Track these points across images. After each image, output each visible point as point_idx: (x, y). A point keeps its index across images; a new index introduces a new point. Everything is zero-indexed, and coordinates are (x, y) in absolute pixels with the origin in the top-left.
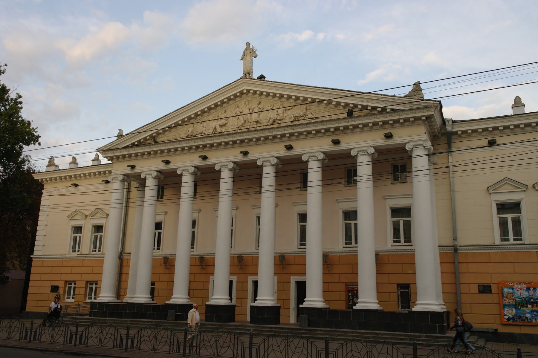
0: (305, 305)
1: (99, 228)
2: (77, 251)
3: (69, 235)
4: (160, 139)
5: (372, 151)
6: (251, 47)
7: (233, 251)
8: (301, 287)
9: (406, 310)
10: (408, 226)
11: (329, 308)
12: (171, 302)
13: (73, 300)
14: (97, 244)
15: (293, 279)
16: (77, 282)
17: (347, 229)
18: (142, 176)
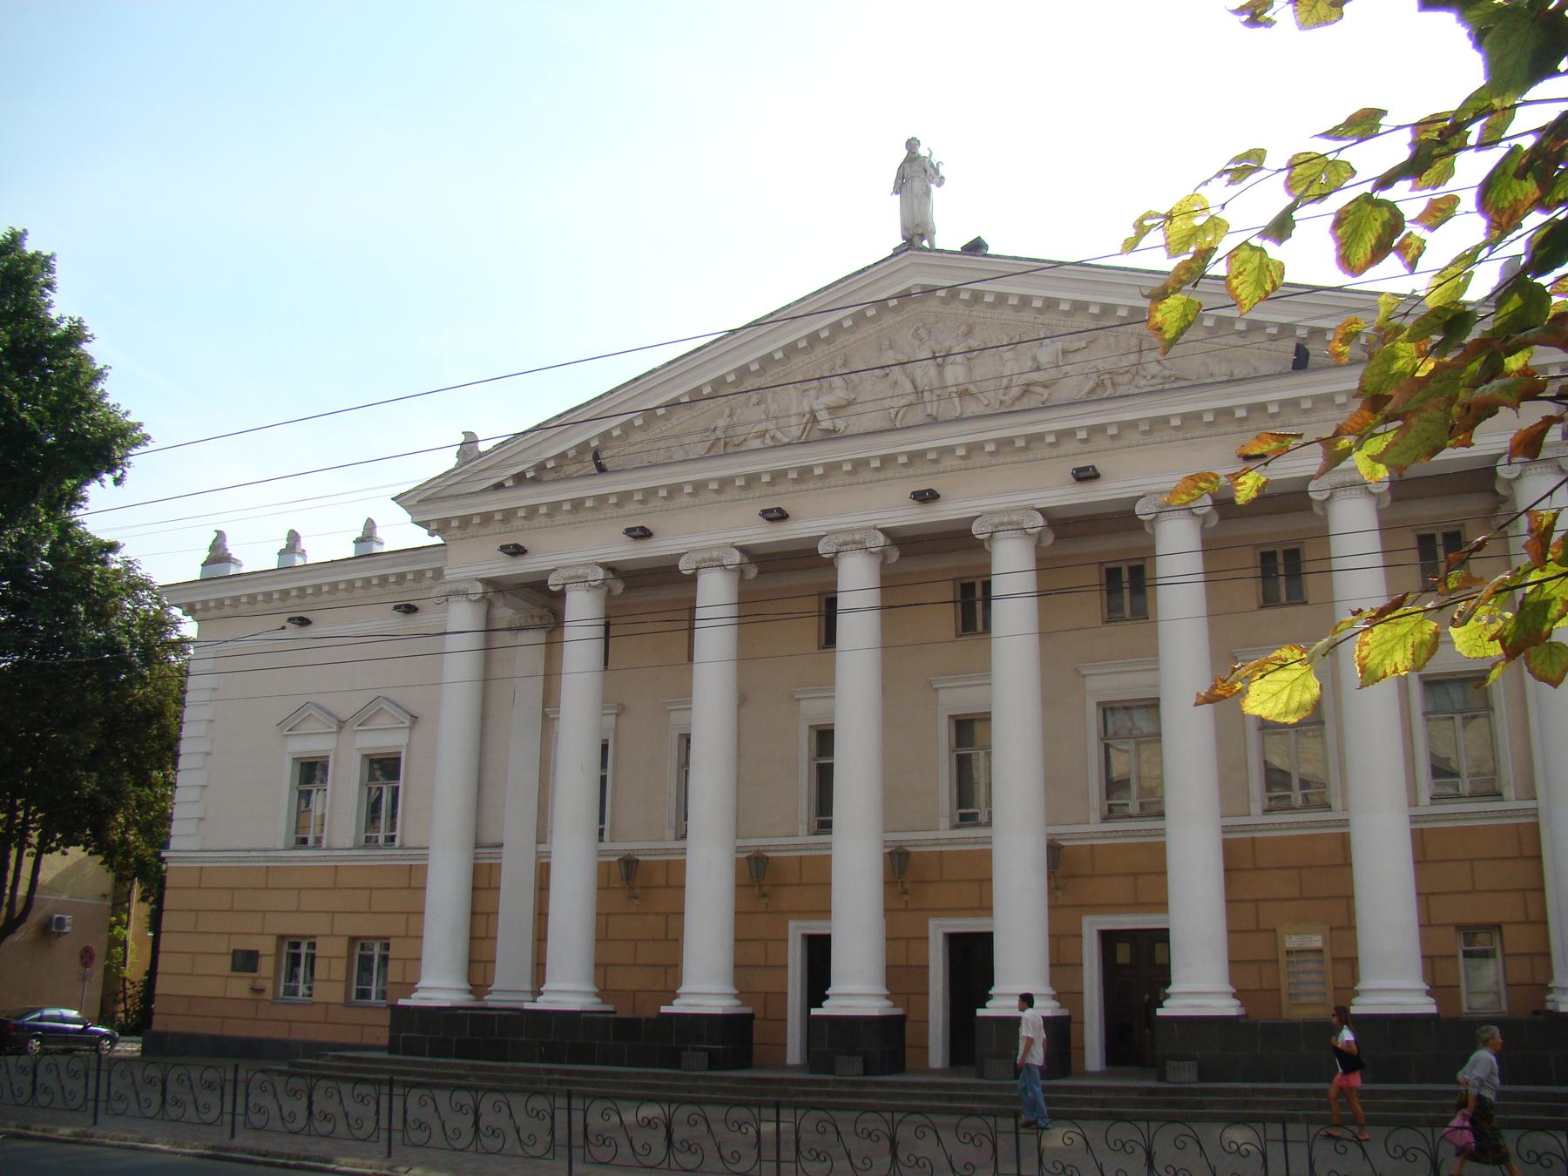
0: (829, 1008)
1: (385, 767)
3: (286, 777)
8: (819, 951)
12: (678, 1007)
14: (379, 812)
15: (938, 929)
16: (392, 942)
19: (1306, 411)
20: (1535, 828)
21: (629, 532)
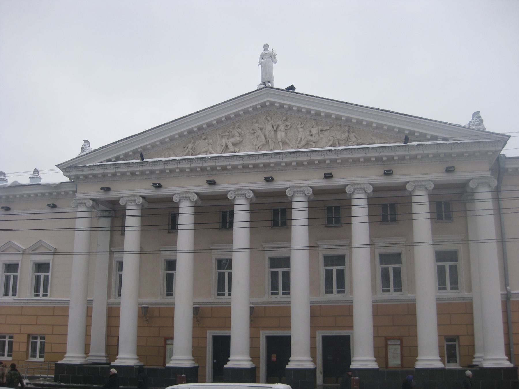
6: (270, 49)
7: (141, 300)
10: (341, 274)
13: (42, 360)
15: (210, 334)
17: (221, 278)
19: (338, 163)
20: (471, 304)
21: (154, 185)
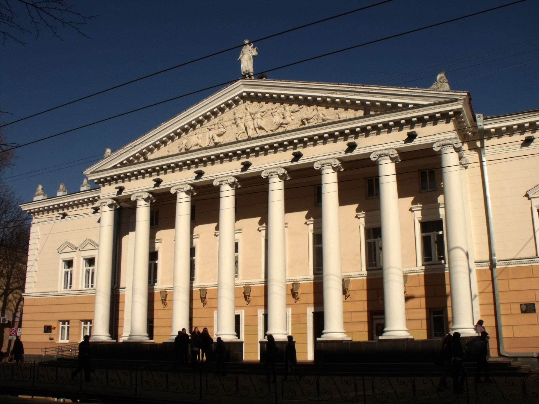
2: (68, 287)
3: (62, 269)
4: (150, 156)
5: (395, 154)
9: (115, 341)
11: (351, 340)
13: (68, 341)
14: (90, 278)
18: (133, 198)
